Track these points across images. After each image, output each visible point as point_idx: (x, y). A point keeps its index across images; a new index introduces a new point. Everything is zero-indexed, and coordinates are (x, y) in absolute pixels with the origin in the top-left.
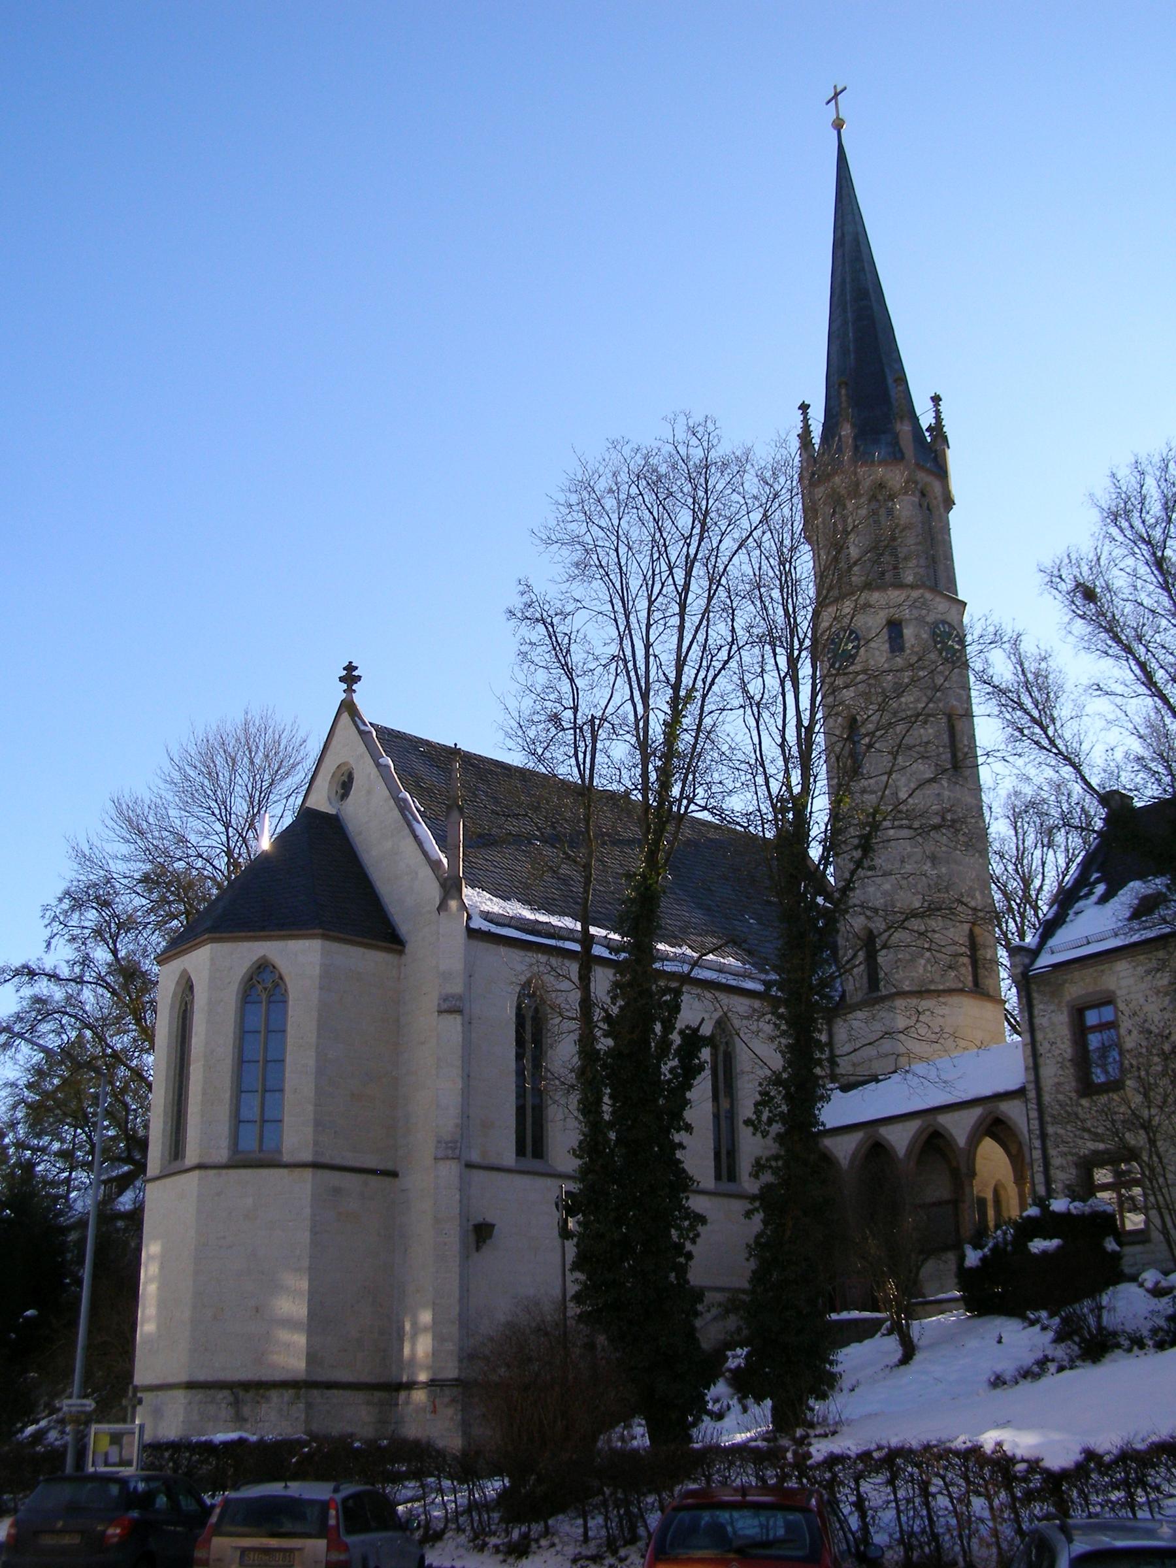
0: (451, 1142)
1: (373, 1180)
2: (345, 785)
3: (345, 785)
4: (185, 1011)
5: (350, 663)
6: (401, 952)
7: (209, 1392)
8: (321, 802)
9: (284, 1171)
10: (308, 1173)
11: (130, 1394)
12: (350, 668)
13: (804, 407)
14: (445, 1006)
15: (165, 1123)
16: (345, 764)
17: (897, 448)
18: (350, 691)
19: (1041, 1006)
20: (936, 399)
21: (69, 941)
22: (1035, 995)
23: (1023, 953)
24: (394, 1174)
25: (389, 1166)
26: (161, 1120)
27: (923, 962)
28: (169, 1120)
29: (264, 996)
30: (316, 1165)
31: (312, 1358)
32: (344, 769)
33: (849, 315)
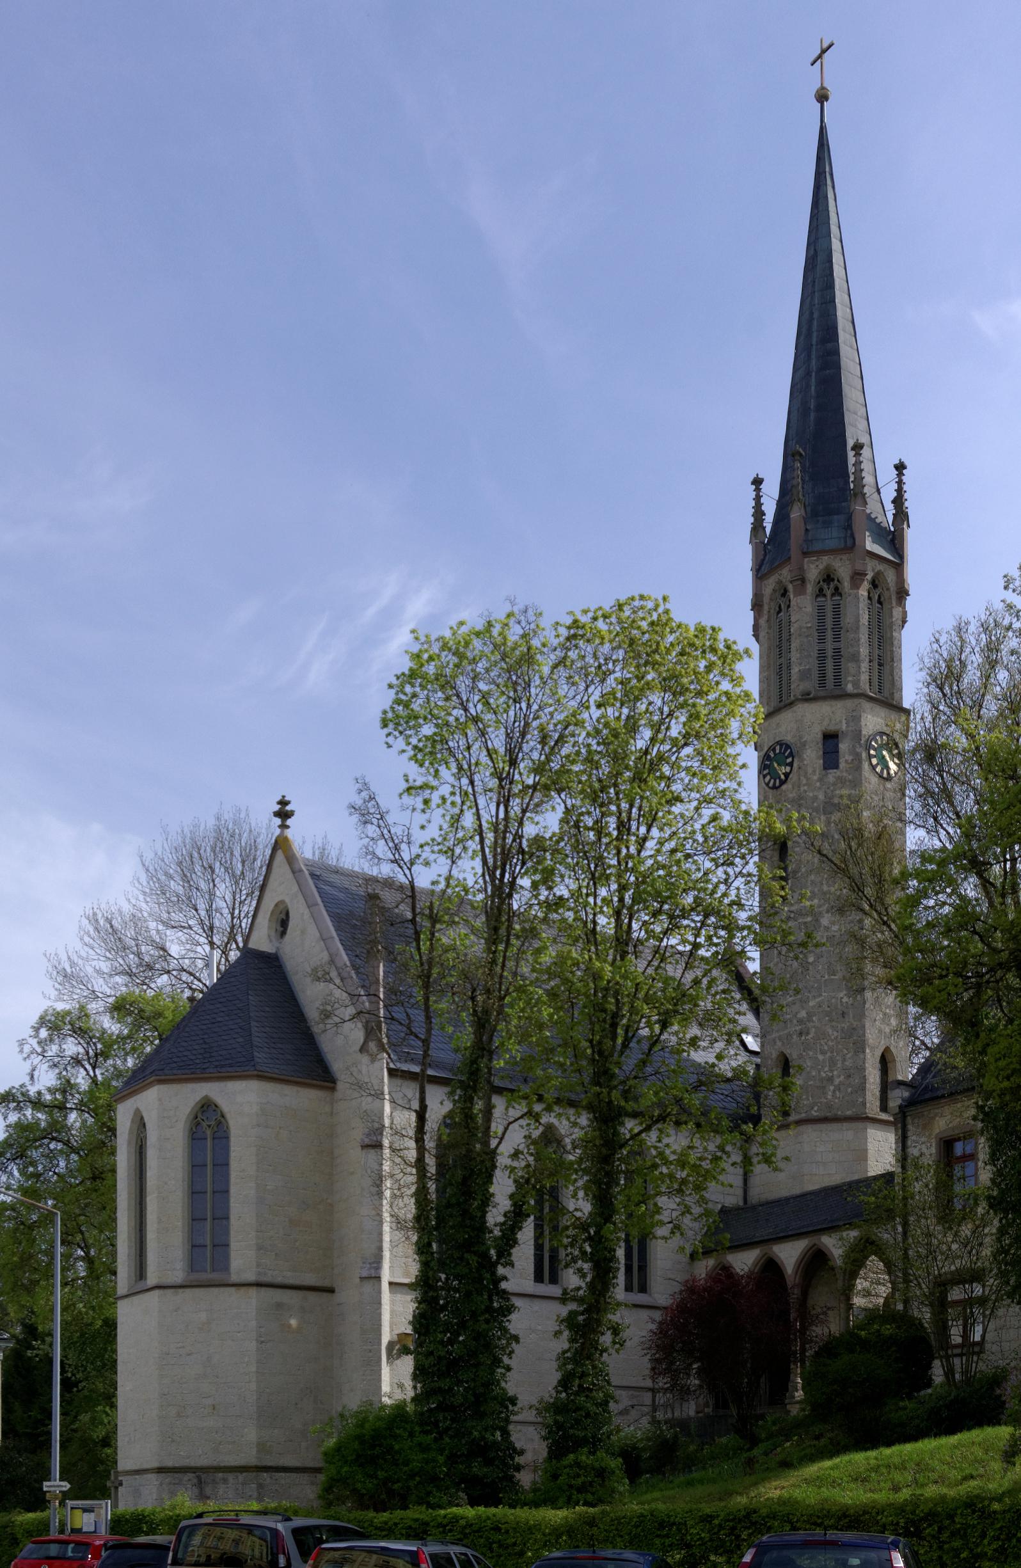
0: (373, 1263)
1: (312, 1297)
2: (283, 923)
3: (283, 923)
4: (141, 1147)
5: (284, 797)
6: (333, 1089)
7: (176, 1475)
8: (262, 941)
9: (233, 1290)
10: (253, 1291)
11: (112, 1478)
12: (283, 803)
13: (757, 482)
14: (367, 1141)
15: (129, 1247)
16: (282, 902)
17: (849, 532)
18: (284, 826)
19: (914, 1138)
20: (900, 467)
21: (50, 1067)
22: (910, 1127)
23: (902, 1087)
24: (331, 1291)
25: (326, 1283)
26: (126, 1244)
27: (832, 1088)
28: (133, 1244)
29: (209, 1132)
30: (259, 1285)
31: (262, 1447)
32: (281, 907)
33: (814, 362)
